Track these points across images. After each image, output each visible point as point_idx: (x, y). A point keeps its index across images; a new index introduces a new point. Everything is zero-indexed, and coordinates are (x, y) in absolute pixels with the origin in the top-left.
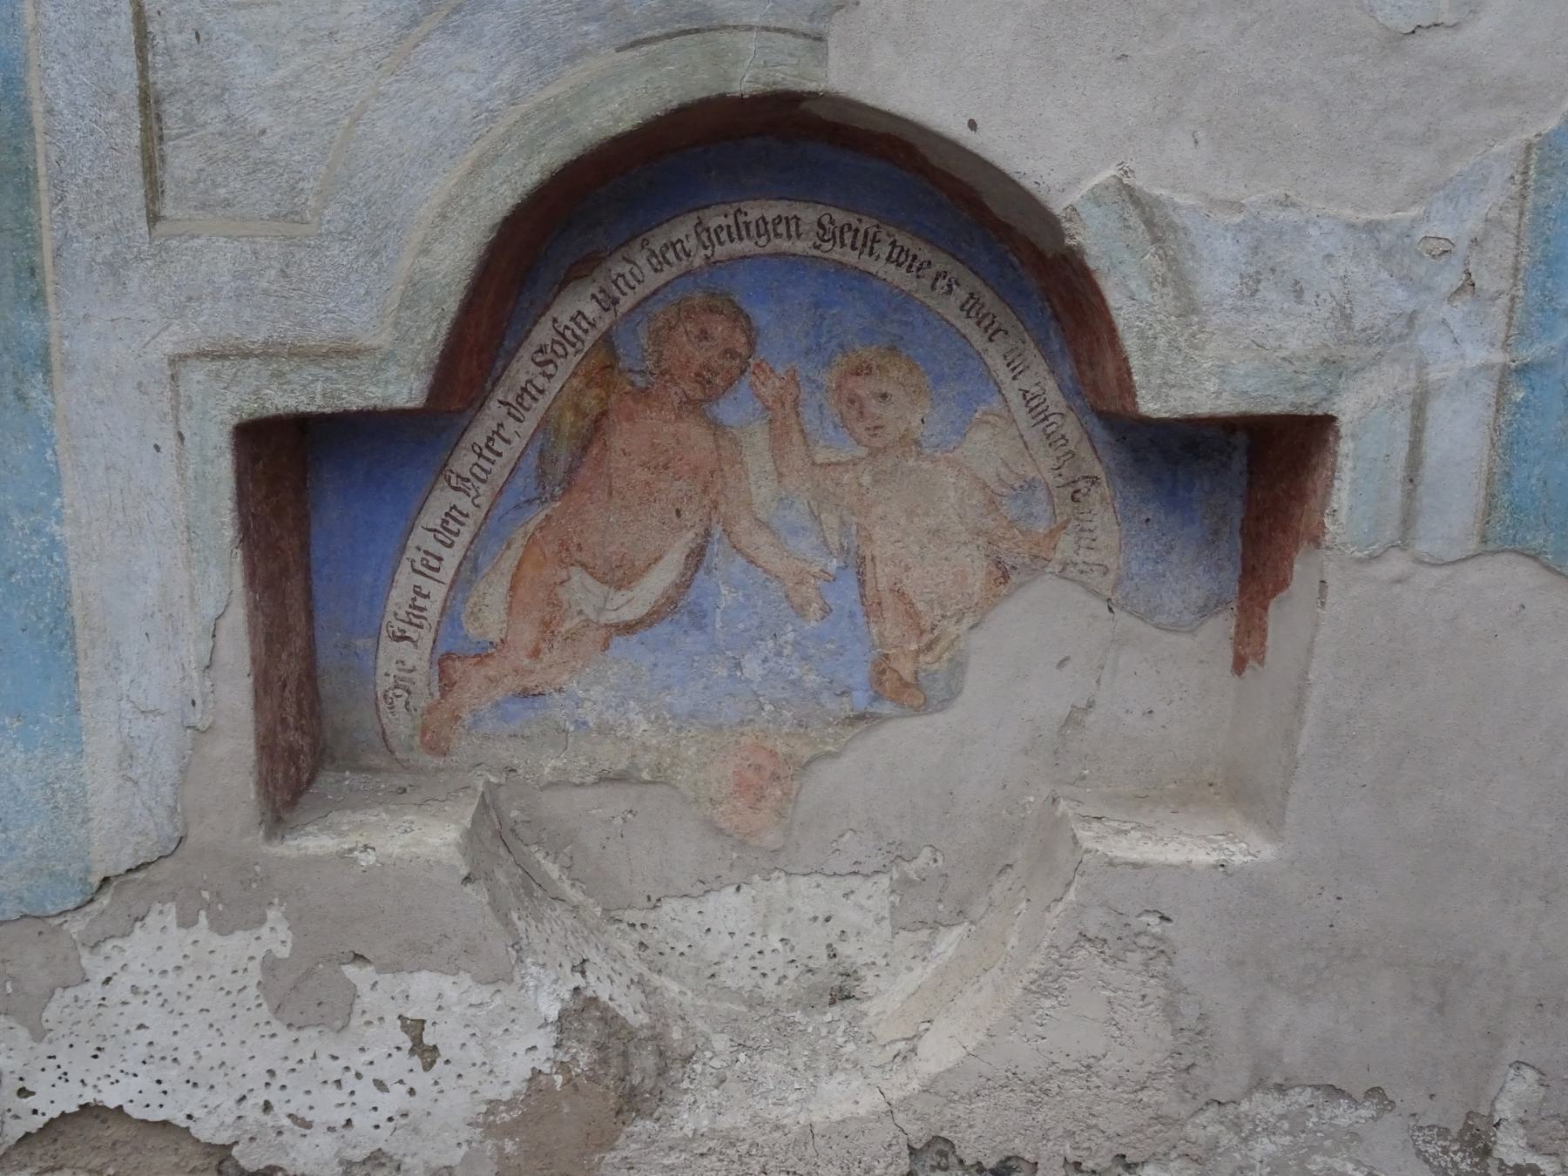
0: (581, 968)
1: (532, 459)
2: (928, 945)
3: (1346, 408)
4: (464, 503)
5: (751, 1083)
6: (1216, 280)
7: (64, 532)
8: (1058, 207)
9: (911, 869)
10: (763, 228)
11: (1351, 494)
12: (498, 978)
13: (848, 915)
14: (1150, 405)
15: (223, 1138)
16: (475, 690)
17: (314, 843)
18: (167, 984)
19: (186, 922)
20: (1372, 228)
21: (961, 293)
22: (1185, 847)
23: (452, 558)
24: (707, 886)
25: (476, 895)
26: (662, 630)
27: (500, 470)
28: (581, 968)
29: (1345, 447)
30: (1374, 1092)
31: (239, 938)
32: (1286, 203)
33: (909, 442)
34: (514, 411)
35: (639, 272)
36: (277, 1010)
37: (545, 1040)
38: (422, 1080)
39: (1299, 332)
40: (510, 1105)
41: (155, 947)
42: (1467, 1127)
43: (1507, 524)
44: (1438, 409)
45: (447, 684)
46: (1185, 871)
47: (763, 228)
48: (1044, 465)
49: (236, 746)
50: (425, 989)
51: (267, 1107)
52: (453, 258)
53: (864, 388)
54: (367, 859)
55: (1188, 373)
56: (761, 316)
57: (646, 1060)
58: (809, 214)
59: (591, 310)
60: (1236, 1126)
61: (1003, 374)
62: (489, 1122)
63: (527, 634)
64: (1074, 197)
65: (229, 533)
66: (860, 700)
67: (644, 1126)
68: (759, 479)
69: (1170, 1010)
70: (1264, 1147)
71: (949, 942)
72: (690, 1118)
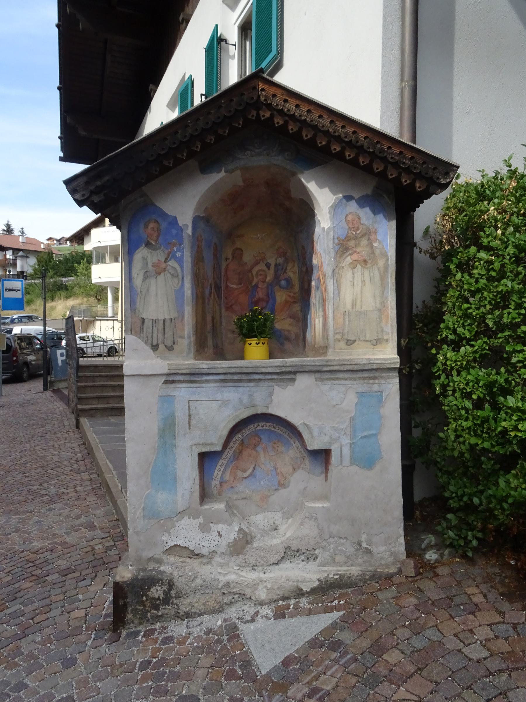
0: (240, 524)
1: (233, 456)
2: (287, 521)
3: (332, 448)
4: (224, 462)
5: (263, 540)
6: (316, 433)
7: (177, 467)
8: (296, 425)
9: (284, 510)
10: (262, 426)
11: (334, 458)
12: (230, 525)
13: (276, 518)
14: (309, 448)
15: (193, 549)
16: (225, 486)
17: (206, 507)
18: (187, 527)
19: (189, 518)
20: (333, 427)
21: (287, 433)
22: (318, 505)
23: (222, 469)
24: (257, 514)
25: (227, 513)
26: (250, 478)
27: (229, 457)
28: (240, 524)
29: (333, 453)
30: (345, 538)
31: (196, 520)
32: (323, 424)
33: (281, 452)
34: (230, 449)
35: (247, 432)
36: (201, 530)
37: (236, 533)
38: (220, 540)
39: (326, 439)
40: (232, 543)
41: (186, 521)
42: (358, 542)
43: (353, 461)
44: (343, 448)
45: (221, 486)
46: (318, 507)
47: (262, 426)
48: (299, 455)
49: (197, 494)
50: (220, 527)
51: (199, 544)
52: (225, 433)
53: (275, 446)
54: (213, 509)
55: (314, 445)
56: (262, 437)
57: (249, 537)
58: (268, 424)
59: (240, 436)
60: (328, 543)
61: (293, 444)
62: (228, 546)
63: (232, 479)
64: (298, 424)
65: (197, 466)
66: (276, 487)
67: (249, 546)
68: (262, 457)
69: (318, 527)
70: (332, 546)
71: (290, 521)
72: (255, 545)
